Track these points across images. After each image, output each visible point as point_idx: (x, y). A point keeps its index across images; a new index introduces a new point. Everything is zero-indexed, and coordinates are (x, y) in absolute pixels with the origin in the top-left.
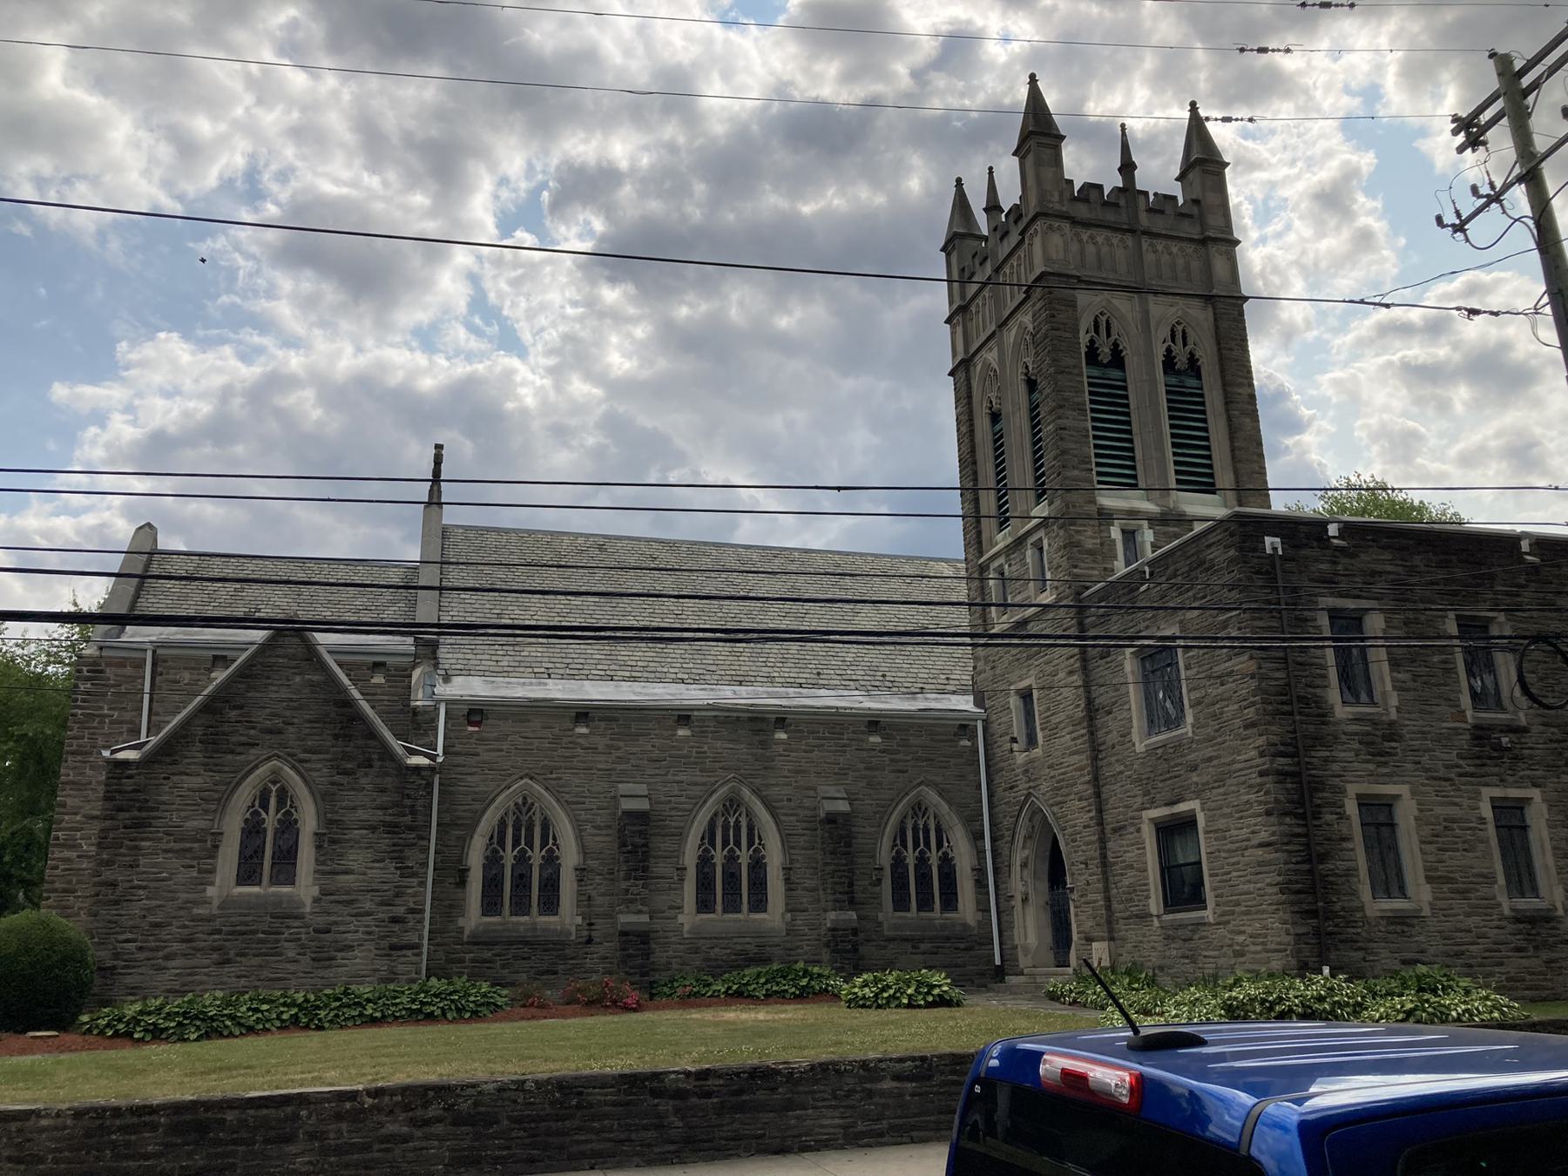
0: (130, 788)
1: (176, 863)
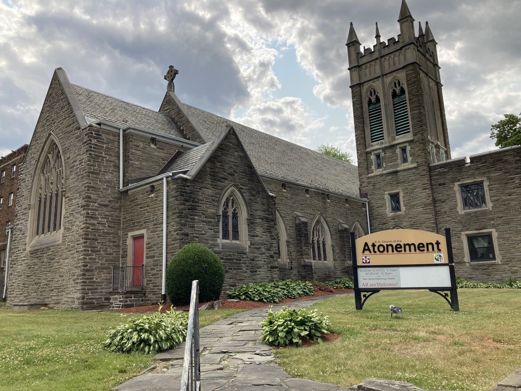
0: (189, 192)
1: (207, 227)
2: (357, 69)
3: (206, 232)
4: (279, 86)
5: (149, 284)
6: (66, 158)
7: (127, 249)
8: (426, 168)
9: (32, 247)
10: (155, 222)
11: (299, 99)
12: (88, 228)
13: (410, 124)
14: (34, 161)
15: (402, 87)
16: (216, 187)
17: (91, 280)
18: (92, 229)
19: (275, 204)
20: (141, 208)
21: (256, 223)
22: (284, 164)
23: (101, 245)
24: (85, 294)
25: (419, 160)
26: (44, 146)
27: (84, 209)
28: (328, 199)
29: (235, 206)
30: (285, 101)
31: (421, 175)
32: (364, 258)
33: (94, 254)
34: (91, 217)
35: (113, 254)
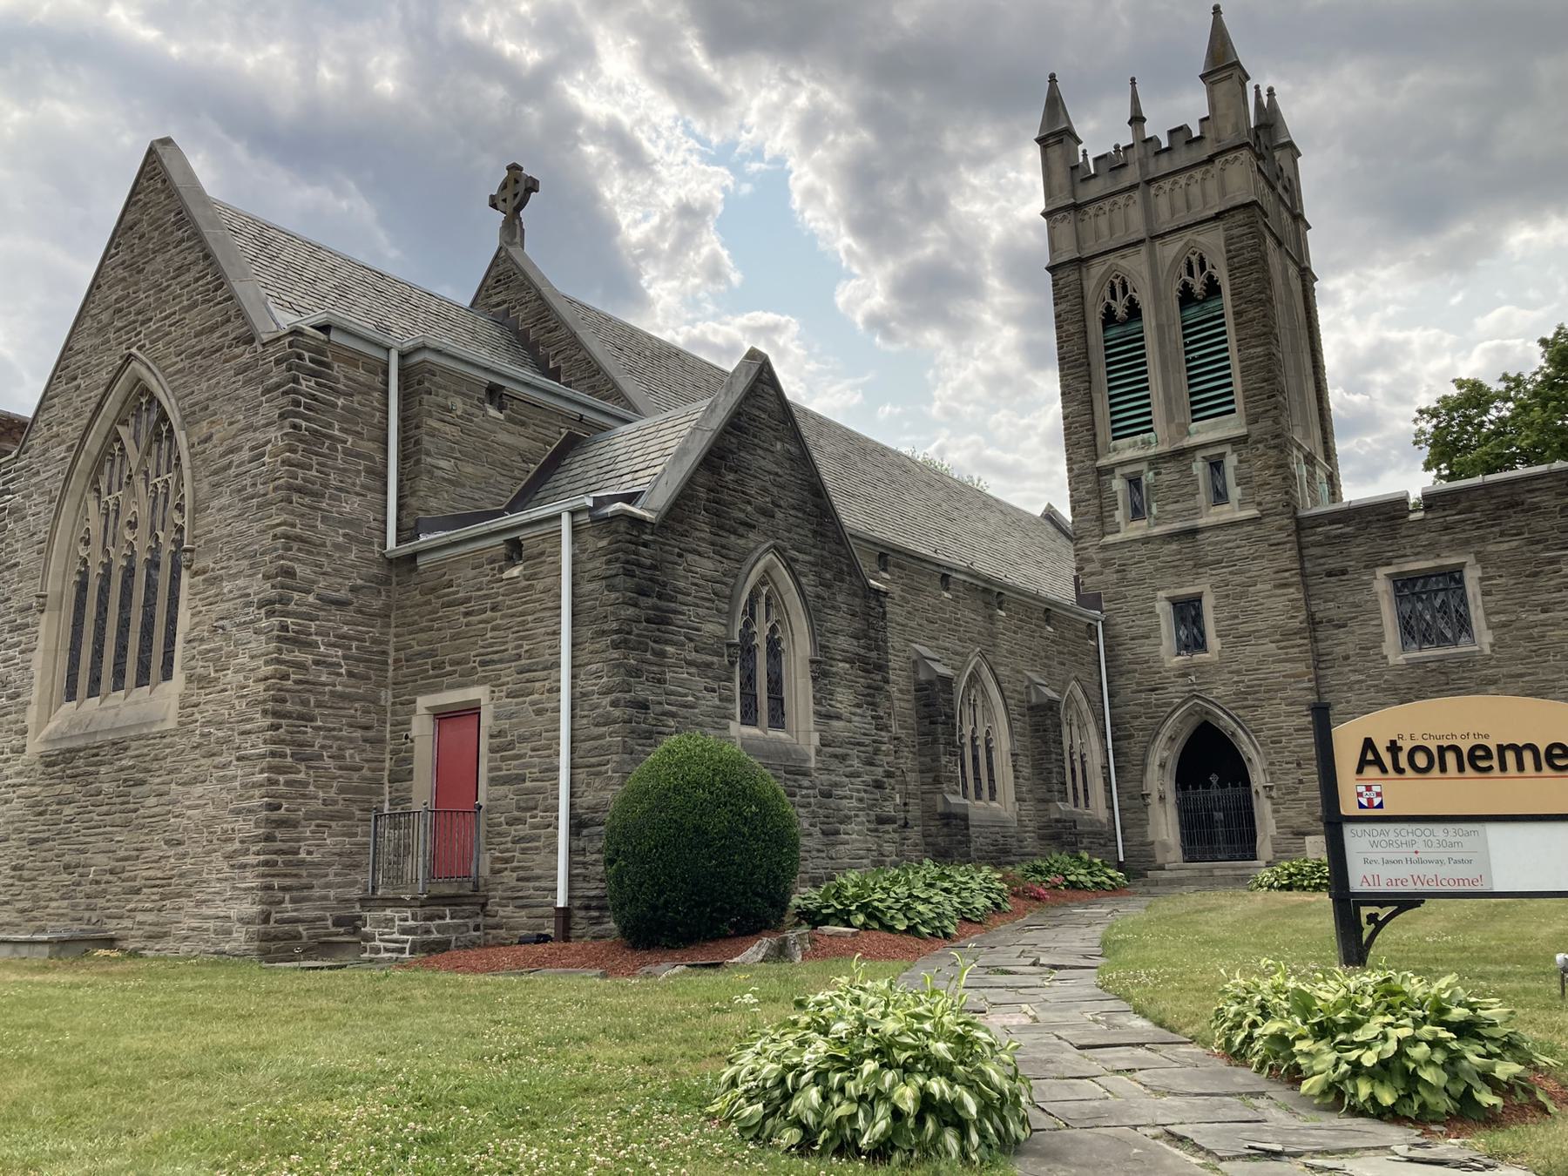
0: (648, 562)
1: (700, 682)
2: (1071, 216)
3: (697, 698)
4: (736, 278)
5: (500, 871)
6: (195, 440)
7: (411, 750)
9: (47, 741)
10: (523, 662)
11: (794, 320)
12: (285, 677)
14: (64, 447)
15: (1210, 277)
16: (724, 551)
17: (290, 857)
18: (297, 682)
19: (885, 613)
20: (467, 614)
21: (836, 674)
23: (325, 738)
24: (271, 904)
25: (1267, 497)
26: (104, 396)
27: (270, 614)
28: (1001, 609)
29: (773, 617)
32: (1362, 789)
33: (302, 767)
34: (295, 641)
35: (361, 769)
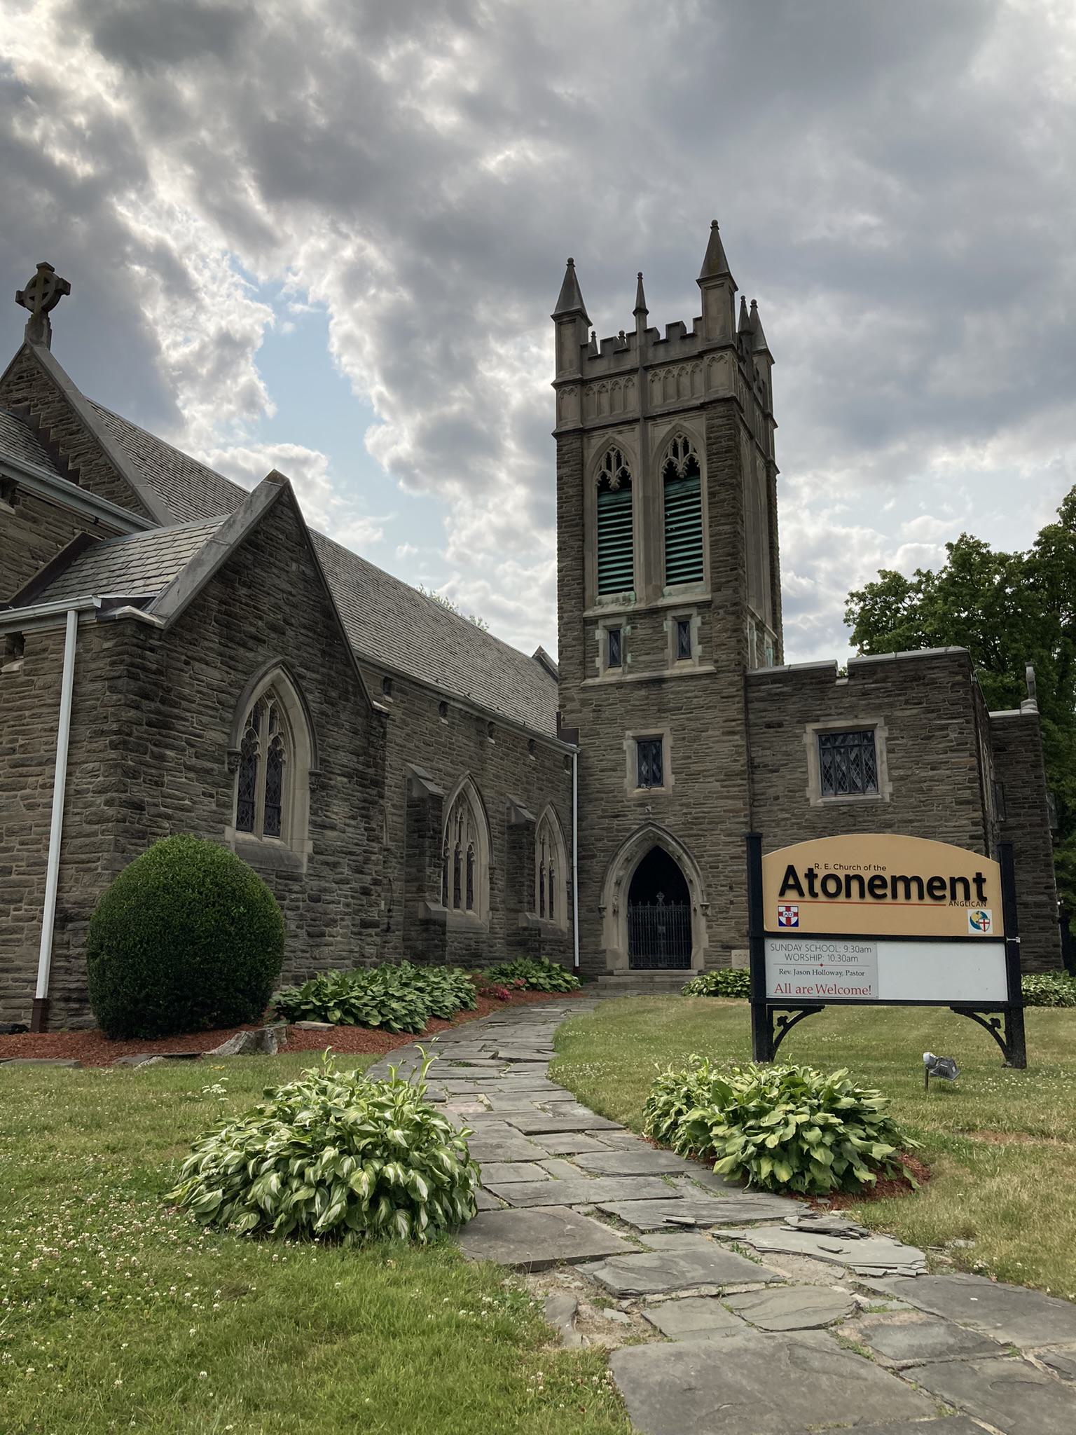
0: (154, 667)
1: (199, 787)
2: (577, 389)
3: (194, 803)
8: (737, 678)
10: (17, 756)
11: (323, 456)
13: (706, 559)
15: (692, 459)
19: (385, 733)
22: (364, 623)
28: (491, 737)
29: (277, 729)
30: (283, 454)
31: (724, 695)
32: (782, 909)
